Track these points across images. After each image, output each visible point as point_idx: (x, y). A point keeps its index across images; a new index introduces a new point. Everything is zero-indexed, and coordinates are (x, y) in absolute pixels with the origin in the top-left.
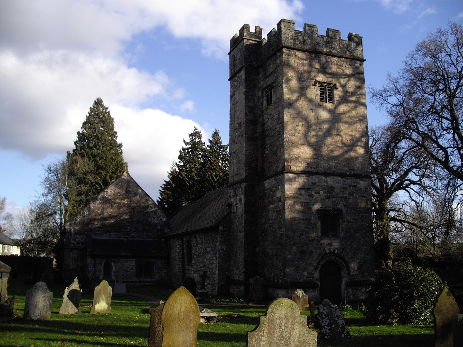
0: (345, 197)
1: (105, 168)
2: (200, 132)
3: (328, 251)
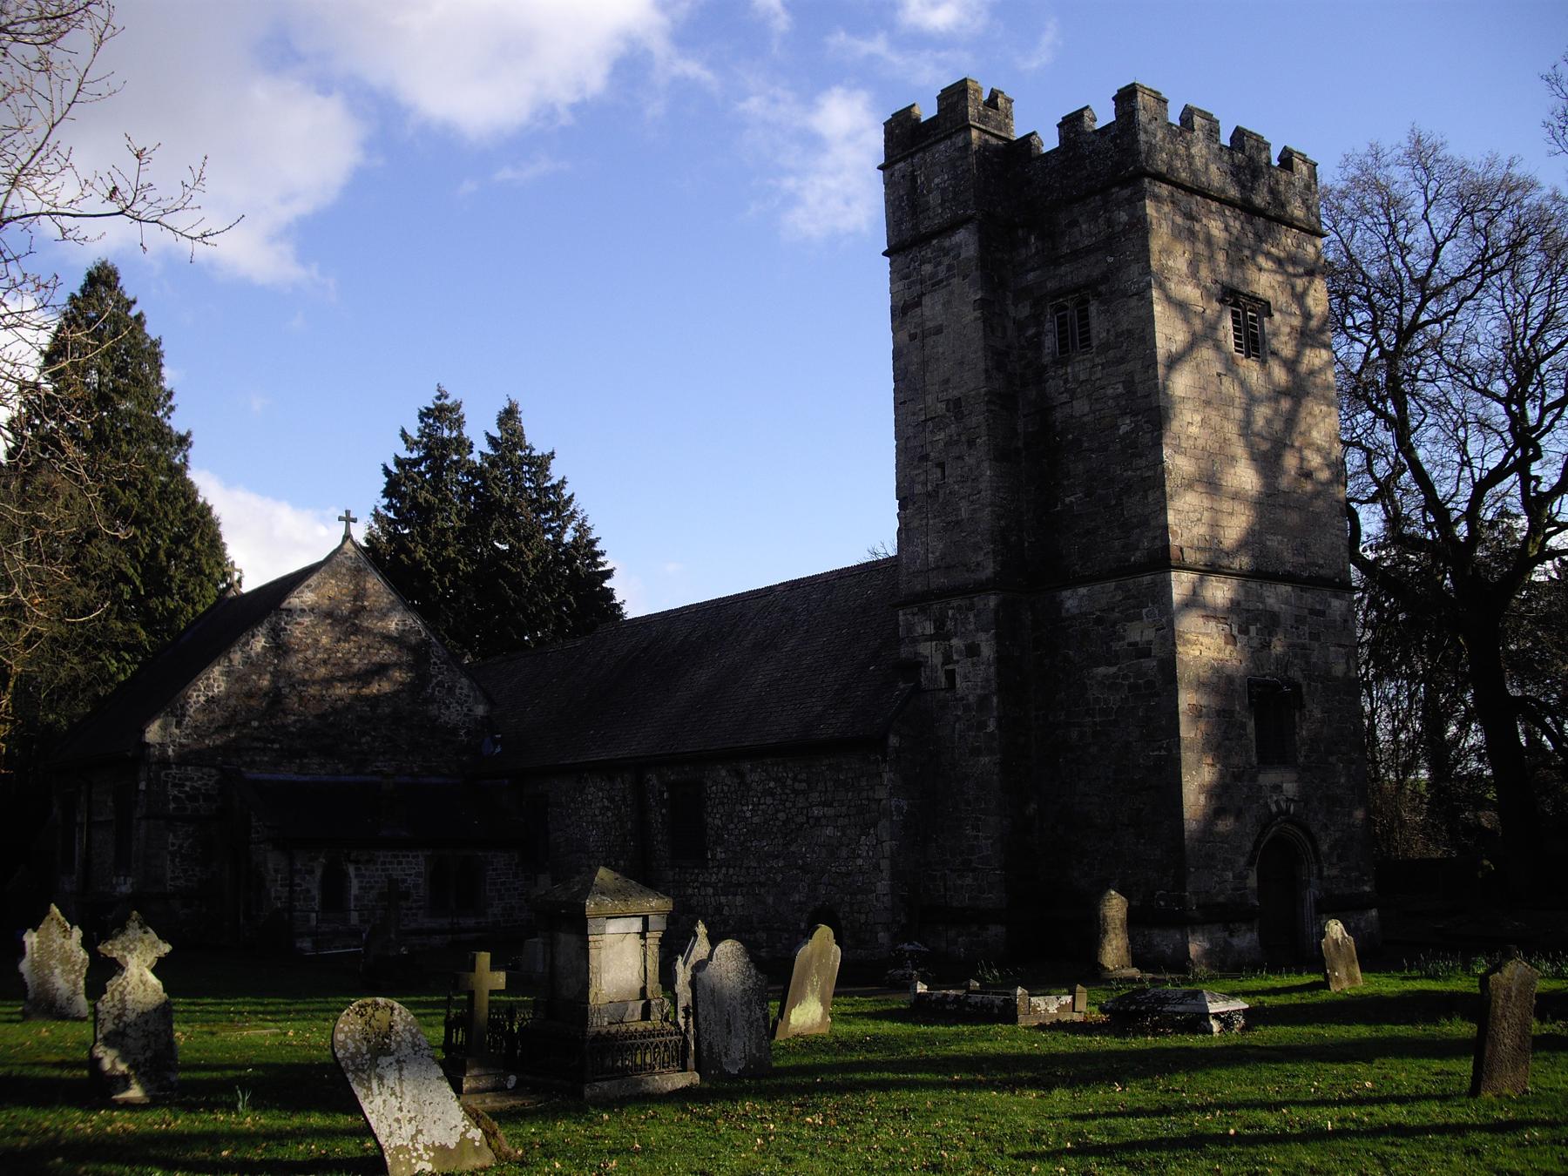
0: (1303, 647)
1: (149, 522)
2: (459, 406)
3: (1274, 808)
